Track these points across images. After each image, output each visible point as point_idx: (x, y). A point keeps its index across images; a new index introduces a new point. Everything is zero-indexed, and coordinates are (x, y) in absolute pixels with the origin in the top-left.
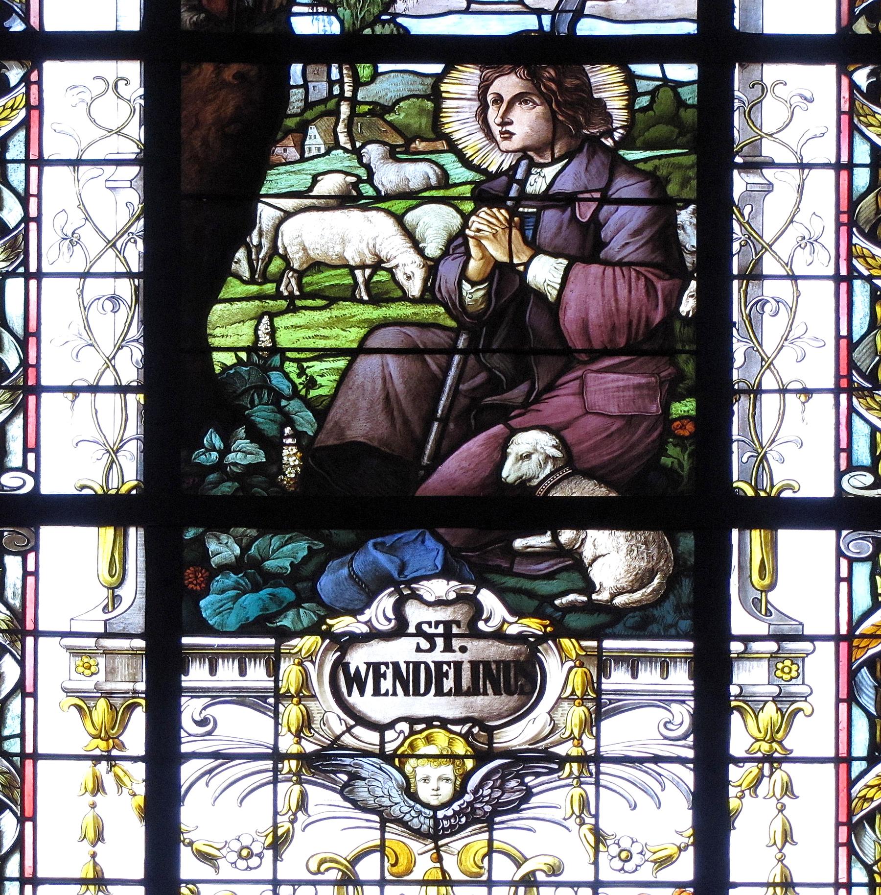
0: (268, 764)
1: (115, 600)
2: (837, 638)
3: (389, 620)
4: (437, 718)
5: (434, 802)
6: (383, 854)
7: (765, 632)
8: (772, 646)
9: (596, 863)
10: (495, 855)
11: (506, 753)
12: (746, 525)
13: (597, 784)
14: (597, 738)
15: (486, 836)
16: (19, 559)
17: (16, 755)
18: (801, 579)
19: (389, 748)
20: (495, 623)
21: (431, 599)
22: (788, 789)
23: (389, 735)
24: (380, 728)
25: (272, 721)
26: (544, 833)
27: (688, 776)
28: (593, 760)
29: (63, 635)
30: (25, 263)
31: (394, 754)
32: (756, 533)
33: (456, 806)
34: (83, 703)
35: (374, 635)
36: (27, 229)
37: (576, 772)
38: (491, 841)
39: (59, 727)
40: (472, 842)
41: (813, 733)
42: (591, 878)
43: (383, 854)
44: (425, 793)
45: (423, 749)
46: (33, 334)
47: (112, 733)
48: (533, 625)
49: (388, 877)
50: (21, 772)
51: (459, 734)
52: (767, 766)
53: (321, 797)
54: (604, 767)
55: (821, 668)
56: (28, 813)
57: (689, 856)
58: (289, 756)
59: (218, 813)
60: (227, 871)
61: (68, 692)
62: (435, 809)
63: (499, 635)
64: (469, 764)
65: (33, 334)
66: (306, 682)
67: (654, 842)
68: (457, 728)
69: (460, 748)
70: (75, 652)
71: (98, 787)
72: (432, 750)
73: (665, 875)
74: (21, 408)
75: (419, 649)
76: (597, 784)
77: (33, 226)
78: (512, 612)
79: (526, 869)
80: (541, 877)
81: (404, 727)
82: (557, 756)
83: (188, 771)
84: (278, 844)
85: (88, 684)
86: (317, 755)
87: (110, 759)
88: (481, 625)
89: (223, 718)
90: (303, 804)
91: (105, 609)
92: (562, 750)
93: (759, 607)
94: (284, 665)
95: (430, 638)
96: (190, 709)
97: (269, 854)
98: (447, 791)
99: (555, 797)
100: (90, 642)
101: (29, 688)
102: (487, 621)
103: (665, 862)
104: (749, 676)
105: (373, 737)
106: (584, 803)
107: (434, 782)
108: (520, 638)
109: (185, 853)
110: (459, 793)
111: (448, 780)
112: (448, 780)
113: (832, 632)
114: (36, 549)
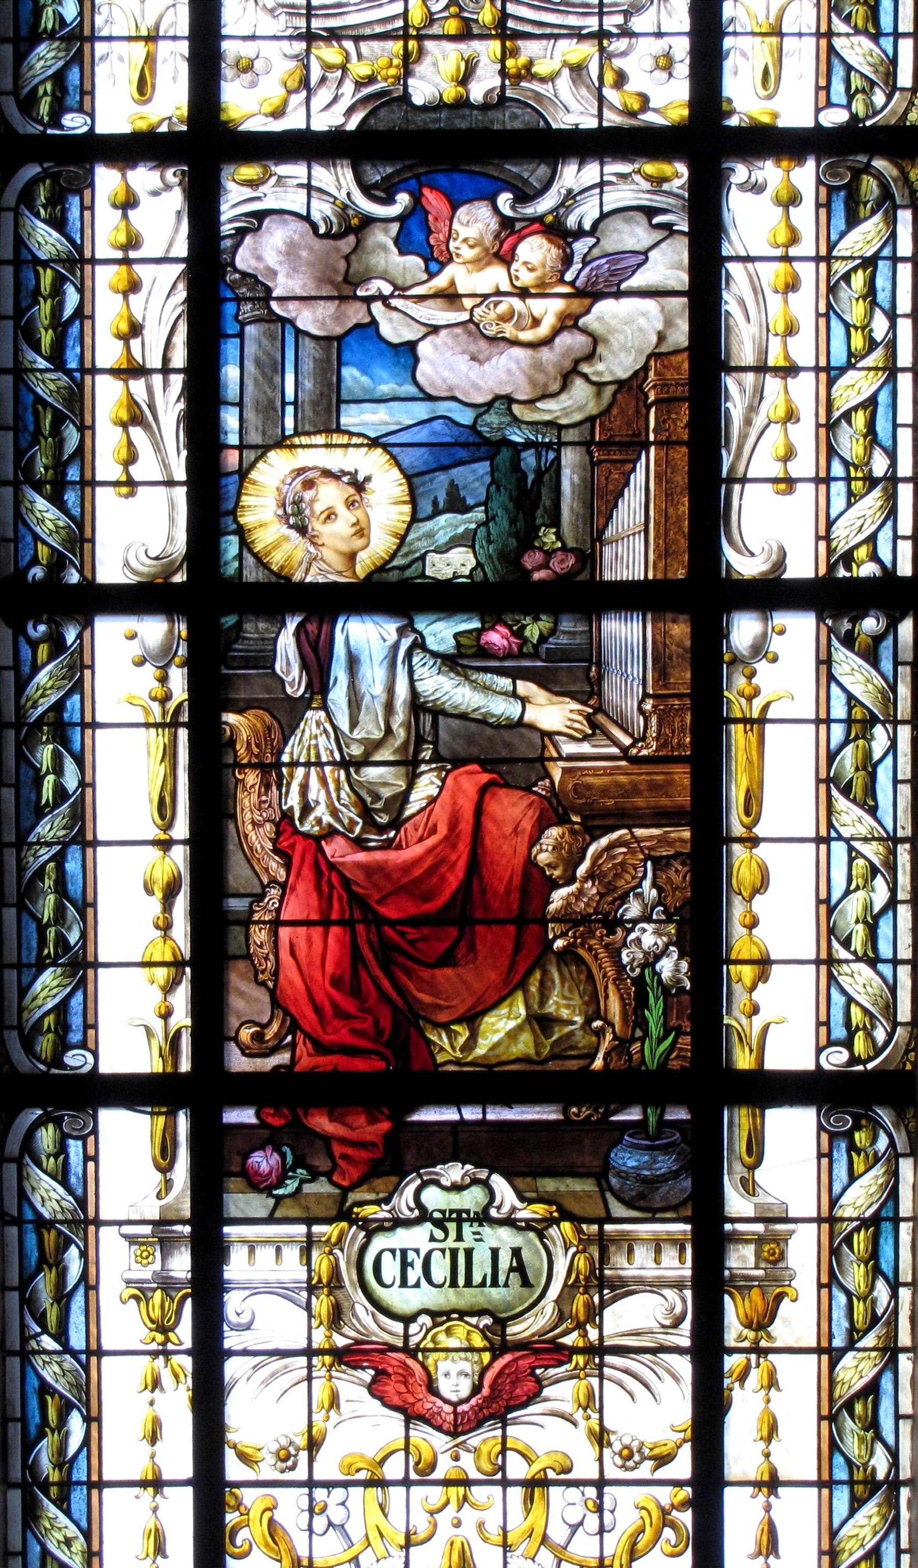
0: (303, 1361)
1: (168, 1184)
2: (819, 1220)
3: (411, 1210)
4: (454, 1311)
5: (454, 1398)
6: (407, 1453)
7: (751, 1213)
8: (759, 1228)
9: (600, 1459)
10: (509, 1453)
11: (522, 1345)
12: (736, 1101)
13: (601, 1377)
14: (600, 1327)
15: (499, 1432)
16: (80, 1143)
17: (82, 1352)
18: (787, 1161)
19: (414, 1341)
20: (505, 1209)
21: (448, 1184)
22: (772, 1382)
23: (414, 1328)
24: (408, 1320)
25: (305, 1314)
26: (546, 1432)
27: (683, 1366)
28: (598, 1350)
29: (120, 1223)
30: (82, 830)
31: (417, 1348)
32: (744, 1111)
33: (473, 1401)
34: (141, 1294)
35: (398, 1223)
36: (83, 794)
37: (581, 1363)
38: (504, 1437)
39: (122, 1323)
40: (485, 1438)
41: (797, 1322)
42: (596, 1476)
43: (407, 1453)
44: (446, 1387)
45: (446, 1341)
46: (822, 315)
47: (164, 1328)
48: (539, 1210)
49: (413, 1476)
50: (86, 1368)
51: (476, 1327)
52: (753, 1357)
53: (353, 1387)
54: (608, 1359)
55: (803, 1251)
56: (94, 1413)
57: (685, 1455)
58: (321, 1352)
59: (259, 1412)
60: (267, 1472)
61: (128, 1282)
62: (455, 1405)
63: (509, 1222)
64: (486, 1357)
65: (822, 315)
66: (335, 1272)
67: (650, 1438)
68: (474, 1320)
69: (478, 1341)
70: (132, 1240)
71: (156, 1384)
72: (453, 1343)
73: (664, 1473)
74: (82, 983)
75: (432, 1239)
76: (601, 1377)
77: (89, 791)
78: (522, 1199)
79: (536, 1467)
80: (551, 1475)
81: (425, 1319)
82: (564, 1347)
83: (232, 1368)
84: (313, 1445)
85: (147, 1274)
86: (347, 1350)
87: (167, 1354)
88: (493, 1213)
89: (265, 1266)
90: (334, 1401)
91: (159, 1196)
92: (568, 1340)
93: (749, 1187)
94: (315, 1254)
95: (439, 1224)
96: (233, 1302)
97: (304, 1456)
98: (465, 1388)
99: (563, 1393)
100: (147, 1229)
101: (92, 1282)
102: (499, 1208)
103: (663, 1460)
104: (741, 1259)
105: (398, 1327)
106: (590, 1396)
107: (455, 1378)
108: (528, 1226)
109: (230, 1456)
110: (476, 1389)
111: (467, 1375)
112: (467, 1375)
113: (815, 1215)
114: (95, 1132)
